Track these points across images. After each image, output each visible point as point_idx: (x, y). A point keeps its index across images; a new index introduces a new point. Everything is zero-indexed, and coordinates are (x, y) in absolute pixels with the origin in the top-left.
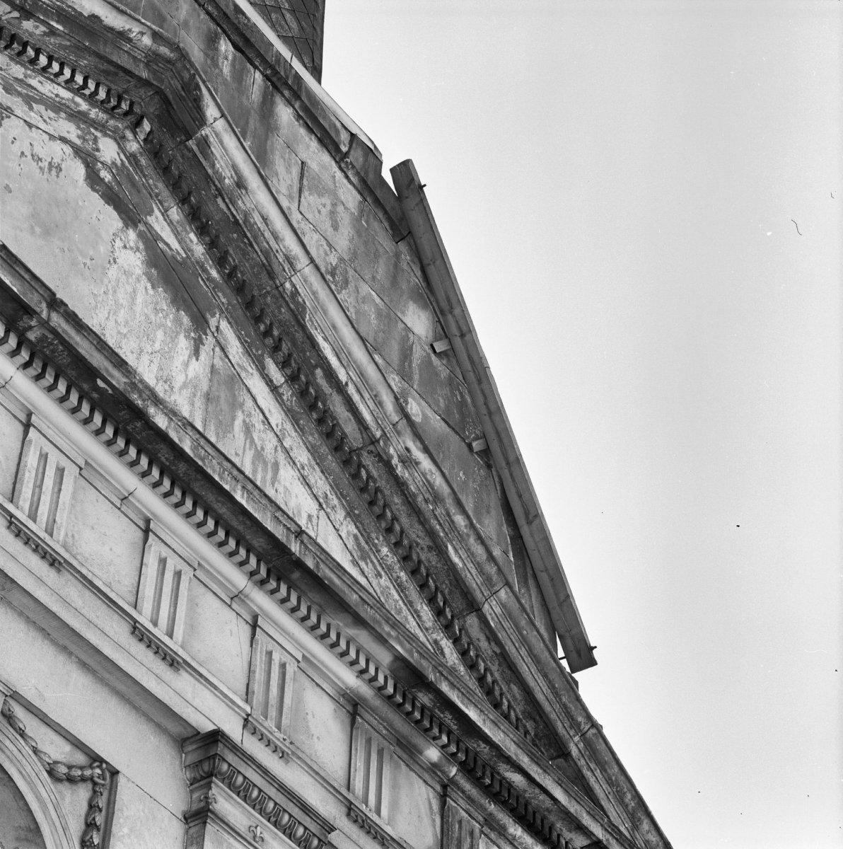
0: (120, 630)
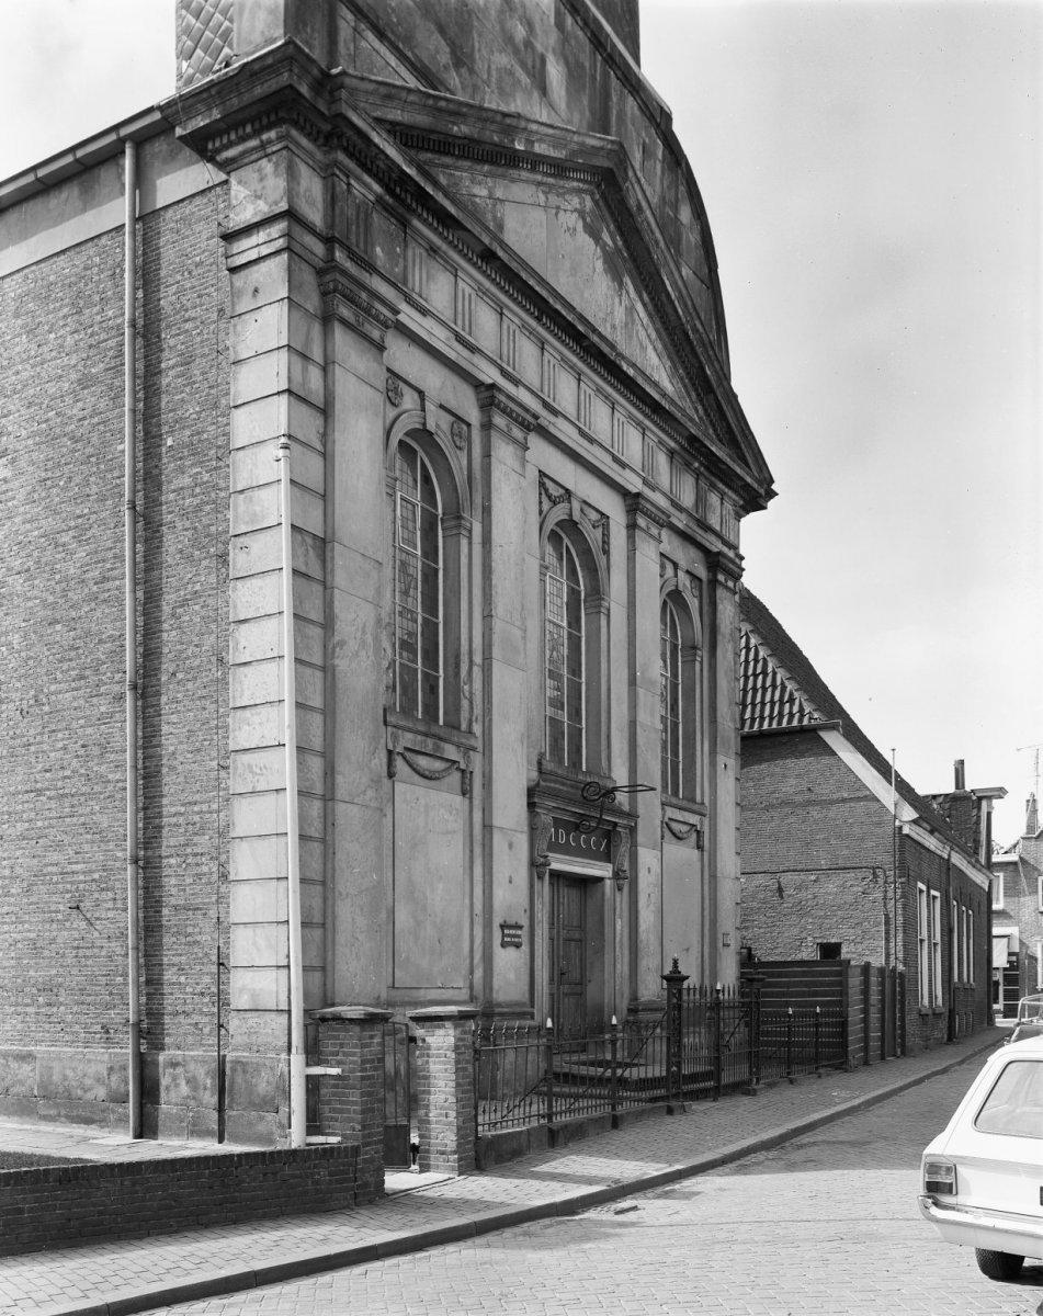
0: (608, 459)
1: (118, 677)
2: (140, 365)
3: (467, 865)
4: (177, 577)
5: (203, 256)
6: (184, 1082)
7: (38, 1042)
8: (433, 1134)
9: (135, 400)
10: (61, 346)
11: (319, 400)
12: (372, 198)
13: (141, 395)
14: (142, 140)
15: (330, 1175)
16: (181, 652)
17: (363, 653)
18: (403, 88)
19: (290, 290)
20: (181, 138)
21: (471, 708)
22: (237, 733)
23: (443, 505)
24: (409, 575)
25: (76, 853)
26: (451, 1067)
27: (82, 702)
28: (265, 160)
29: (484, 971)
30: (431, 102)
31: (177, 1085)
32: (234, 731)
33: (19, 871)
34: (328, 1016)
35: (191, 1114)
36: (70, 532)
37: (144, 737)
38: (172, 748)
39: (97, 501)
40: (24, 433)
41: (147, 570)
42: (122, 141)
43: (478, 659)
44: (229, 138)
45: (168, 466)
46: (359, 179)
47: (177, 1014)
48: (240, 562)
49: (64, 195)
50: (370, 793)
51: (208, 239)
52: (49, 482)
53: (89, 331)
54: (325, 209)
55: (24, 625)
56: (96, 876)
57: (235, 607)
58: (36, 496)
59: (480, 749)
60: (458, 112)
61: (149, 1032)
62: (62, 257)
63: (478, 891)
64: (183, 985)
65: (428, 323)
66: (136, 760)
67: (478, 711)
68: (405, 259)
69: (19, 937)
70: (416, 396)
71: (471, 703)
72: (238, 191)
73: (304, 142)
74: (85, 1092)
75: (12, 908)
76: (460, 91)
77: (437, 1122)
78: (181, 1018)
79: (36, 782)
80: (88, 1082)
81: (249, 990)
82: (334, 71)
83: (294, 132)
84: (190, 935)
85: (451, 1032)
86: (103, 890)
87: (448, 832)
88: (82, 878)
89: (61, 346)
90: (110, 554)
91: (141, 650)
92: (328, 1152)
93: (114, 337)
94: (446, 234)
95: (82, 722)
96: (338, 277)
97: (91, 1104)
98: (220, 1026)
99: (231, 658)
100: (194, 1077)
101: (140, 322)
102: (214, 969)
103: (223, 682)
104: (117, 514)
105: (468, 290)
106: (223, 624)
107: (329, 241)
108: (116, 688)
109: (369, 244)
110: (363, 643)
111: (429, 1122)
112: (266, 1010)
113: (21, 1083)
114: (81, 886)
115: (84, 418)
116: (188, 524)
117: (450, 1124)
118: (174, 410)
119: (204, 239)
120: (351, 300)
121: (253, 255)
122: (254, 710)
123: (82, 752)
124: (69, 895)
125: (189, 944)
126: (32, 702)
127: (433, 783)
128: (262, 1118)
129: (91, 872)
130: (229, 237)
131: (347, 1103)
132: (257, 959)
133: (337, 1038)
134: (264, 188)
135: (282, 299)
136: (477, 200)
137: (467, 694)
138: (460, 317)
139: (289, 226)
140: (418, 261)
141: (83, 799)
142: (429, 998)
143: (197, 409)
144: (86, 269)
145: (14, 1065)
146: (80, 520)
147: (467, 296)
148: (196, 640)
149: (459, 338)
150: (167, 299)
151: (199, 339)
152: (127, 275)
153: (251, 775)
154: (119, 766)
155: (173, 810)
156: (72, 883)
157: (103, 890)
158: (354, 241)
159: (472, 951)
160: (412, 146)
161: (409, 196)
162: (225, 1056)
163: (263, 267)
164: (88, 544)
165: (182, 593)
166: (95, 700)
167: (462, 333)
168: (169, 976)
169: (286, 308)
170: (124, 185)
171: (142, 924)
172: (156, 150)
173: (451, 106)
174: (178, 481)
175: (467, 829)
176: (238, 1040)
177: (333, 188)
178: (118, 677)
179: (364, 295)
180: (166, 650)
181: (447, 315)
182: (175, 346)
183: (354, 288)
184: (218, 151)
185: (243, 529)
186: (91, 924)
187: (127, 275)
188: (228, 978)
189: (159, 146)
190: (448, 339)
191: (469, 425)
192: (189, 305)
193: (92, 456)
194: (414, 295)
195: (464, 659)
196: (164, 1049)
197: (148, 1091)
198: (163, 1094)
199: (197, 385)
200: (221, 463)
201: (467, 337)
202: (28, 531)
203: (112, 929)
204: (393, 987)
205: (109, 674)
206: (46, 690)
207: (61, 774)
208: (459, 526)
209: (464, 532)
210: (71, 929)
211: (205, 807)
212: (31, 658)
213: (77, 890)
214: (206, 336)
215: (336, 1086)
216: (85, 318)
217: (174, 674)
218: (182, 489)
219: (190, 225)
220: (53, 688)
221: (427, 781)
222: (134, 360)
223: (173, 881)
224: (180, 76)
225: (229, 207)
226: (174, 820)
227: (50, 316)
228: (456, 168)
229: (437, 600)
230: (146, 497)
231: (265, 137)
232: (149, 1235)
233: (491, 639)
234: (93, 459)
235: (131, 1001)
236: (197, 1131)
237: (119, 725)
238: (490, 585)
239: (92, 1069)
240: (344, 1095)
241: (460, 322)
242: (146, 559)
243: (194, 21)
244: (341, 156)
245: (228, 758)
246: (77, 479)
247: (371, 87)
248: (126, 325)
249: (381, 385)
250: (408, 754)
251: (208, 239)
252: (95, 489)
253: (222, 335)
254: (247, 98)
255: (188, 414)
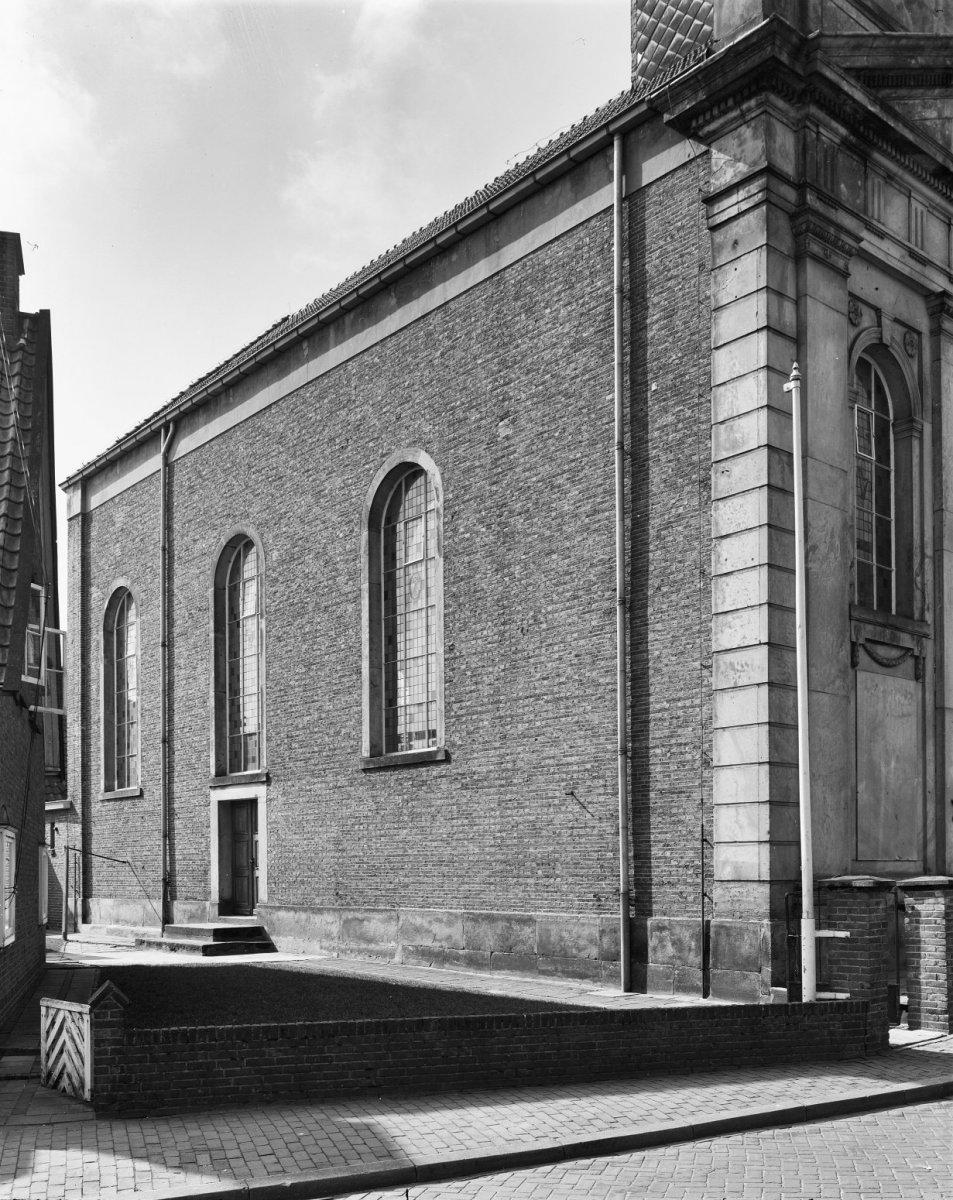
1: (607, 594)
2: (627, 325)
3: (920, 746)
4: (662, 503)
5: (684, 221)
6: (670, 944)
7: (537, 908)
8: (923, 994)
9: (622, 355)
10: (556, 318)
11: (791, 331)
12: (837, 140)
13: (628, 350)
14: (626, 133)
15: (845, 1026)
16: (665, 568)
17: (832, 555)
18: (870, 36)
19: (768, 238)
20: (670, 123)
21: (923, 597)
22: (718, 636)
23: (894, 410)
24: (865, 479)
25: (571, 747)
26: (941, 932)
27: (576, 618)
28: (743, 128)
29: (937, 845)
30: (893, 43)
31: (664, 947)
32: (716, 634)
33: (520, 764)
34: (836, 885)
35: (676, 972)
36: (564, 475)
37: (632, 645)
38: (657, 653)
39: (589, 445)
40: (523, 396)
41: (634, 501)
42: (611, 136)
43: (929, 551)
44: (711, 114)
45: (653, 408)
46: (827, 126)
47: (662, 884)
48: (721, 484)
49: (558, 190)
50: (838, 683)
51: (689, 205)
52: (546, 435)
53: (581, 302)
54: (797, 159)
55: (524, 557)
56: (588, 766)
57: (717, 524)
58: (534, 448)
59: (932, 636)
60: (916, 47)
61: (639, 899)
62: (556, 243)
63: (931, 768)
64: (669, 859)
65: (885, 245)
66: (624, 664)
67: (929, 600)
68: (865, 190)
69: (520, 819)
70: (873, 313)
71: (923, 593)
72: (718, 157)
73: (781, 103)
74: (580, 951)
75: (515, 796)
76: (911, 28)
77: (927, 984)
78: (667, 889)
79: (535, 689)
80: (582, 943)
81: (732, 863)
82: (811, 36)
83: (772, 97)
84: (674, 815)
85: (941, 900)
86: (594, 778)
87: (903, 715)
88: (575, 768)
89: (556, 318)
90: (600, 490)
91: (629, 569)
92: (840, 1006)
93: (603, 303)
94: (903, 160)
95: (575, 635)
96: (811, 218)
97: (585, 962)
98: (704, 895)
99: (714, 570)
100: (679, 940)
101: (627, 287)
102: (698, 845)
103: (706, 592)
104: (607, 455)
105: (920, 208)
106: (706, 541)
107: (800, 187)
108: (606, 604)
109: (835, 183)
110: (831, 547)
111: (919, 983)
112: (747, 881)
113: (523, 943)
114: (575, 776)
115: (577, 376)
116: (671, 457)
117: (940, 986)
118: (658, 359)
119: (686, 205)
120: (821, 236)
121: (733, 212)
122: (735, 615)
123: (575, 661)
124: (563, 784)
125: (674, 823)
126: (531, 622)
127: (885, 670)
128: (745, 977)
129: (583, 762)
130: (710, 200)
131: (856, 963)
132: (739, 835)
133: (845, 904)
134: (743, 151)
135: (761, 247)
136: (928, 123)
137: (919, 585)
138: (913, 234)
139: (768, 182)
140: (876, 189)
141: (576, 701)
142: (887, 870)
143: (680, 355)
144: (577, 249)
145: (516, 927)
146: (573, 464)
147: (919, 214)
148: (679, 557)
149: (912, 254)
150: (652, 263)
151: (680, 294)
152: (615, 248)
153: (733, 672)
154: (609, 671)
155: (658, 706)
156: (567, 773)
157: (594, 778)
158: (822, 182)
159: (925, 825)
160: (874, 87)
161: (871, 133)
162: (709, 922)
163: (742, 221)
164: (580, 483)
165: (666, 517)
166: (587, 616)
167: (916, 249)
168: (656, 851)
169: (764, 254)
170: (612, 173)
171: (630, 806)
172: (641, 137)
173: (911, 42)
174: (661, 421)
175: (920, 712)
176: (721, 907)
177: (805, 139)
178: (607, 594)
179: (832, 230)
180: (651, 568)
181: (901, 236)
182: (658, 303)
183: (823, 225)
184: (701, 127)
185: (725, 455)
186: (585, 808)
187: (615, 248)
188: (712, 853)
189: (644, 133)
190: (903, 256)
191: (919, 333)
192: (671, 265)
193: (584, 407)
194: (875, 223)
195: (917, 551)
196: (651, 915)
197: (637, 951)
198: (650, 954)
199: (679, 334)
200: (703, 400)
201: (921, 252)
202: (527, 478)
203: (602, 811)
204: (857, 860)
205: (599, 593)
206: (543, 611)
207: (557, 680)
208: (912, 429)
209: (916, 434)
210: (566, 812)
211: (688, 703)
212: (531, 584)
213: (572, 779)
214: (687, 290)
215: (842, 948)
216: (577, 291)
217: (659, 588)
218: (666, 426)
219: (672, 195)
220: (549, 608)
221: (884, 668)
222: (622, 320)
223: (659, 768)
224: (635, 68)
225: (710, 173)
226: (660, 715)
227: (546, 295)
228: (910, 98)
229: (889, 500)
230: (632, 437)
231: (744, 107)
232: (692, 1072)
233: (942, 532)
234: (585, 411)
235: (621, 873)
236: (682, 987)
237: (609, 635)
238: (941, 482)
239: (586, 932)
240: (853, 956)
241: (913, 238)
242: (633, 489)
243: (647, 17)
244: (813, 110)
245: (710, 658)
246: (571, 429)
247: (842, 42)
248: (615, 291)
249: (844, 308)
250: (868, 645)
251: (689, 205)
252: (586, 435)
253: (703, 286)
254: (731, 76)
255: (670, 361)
